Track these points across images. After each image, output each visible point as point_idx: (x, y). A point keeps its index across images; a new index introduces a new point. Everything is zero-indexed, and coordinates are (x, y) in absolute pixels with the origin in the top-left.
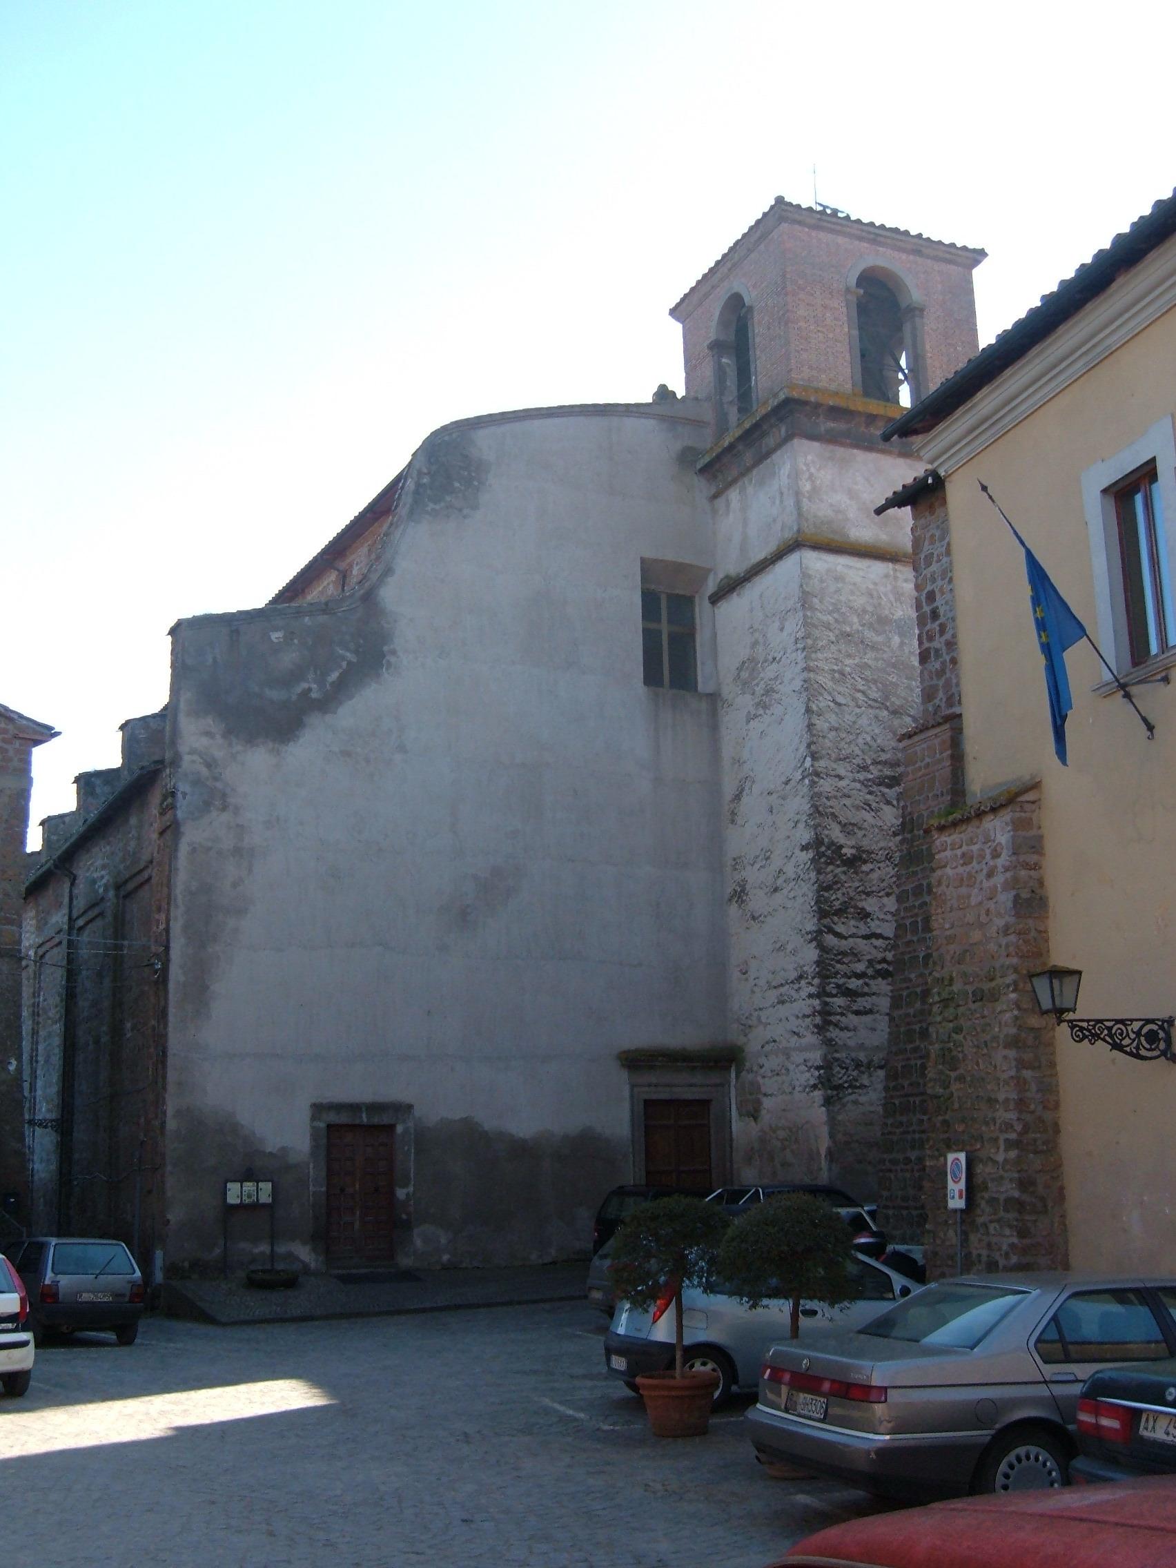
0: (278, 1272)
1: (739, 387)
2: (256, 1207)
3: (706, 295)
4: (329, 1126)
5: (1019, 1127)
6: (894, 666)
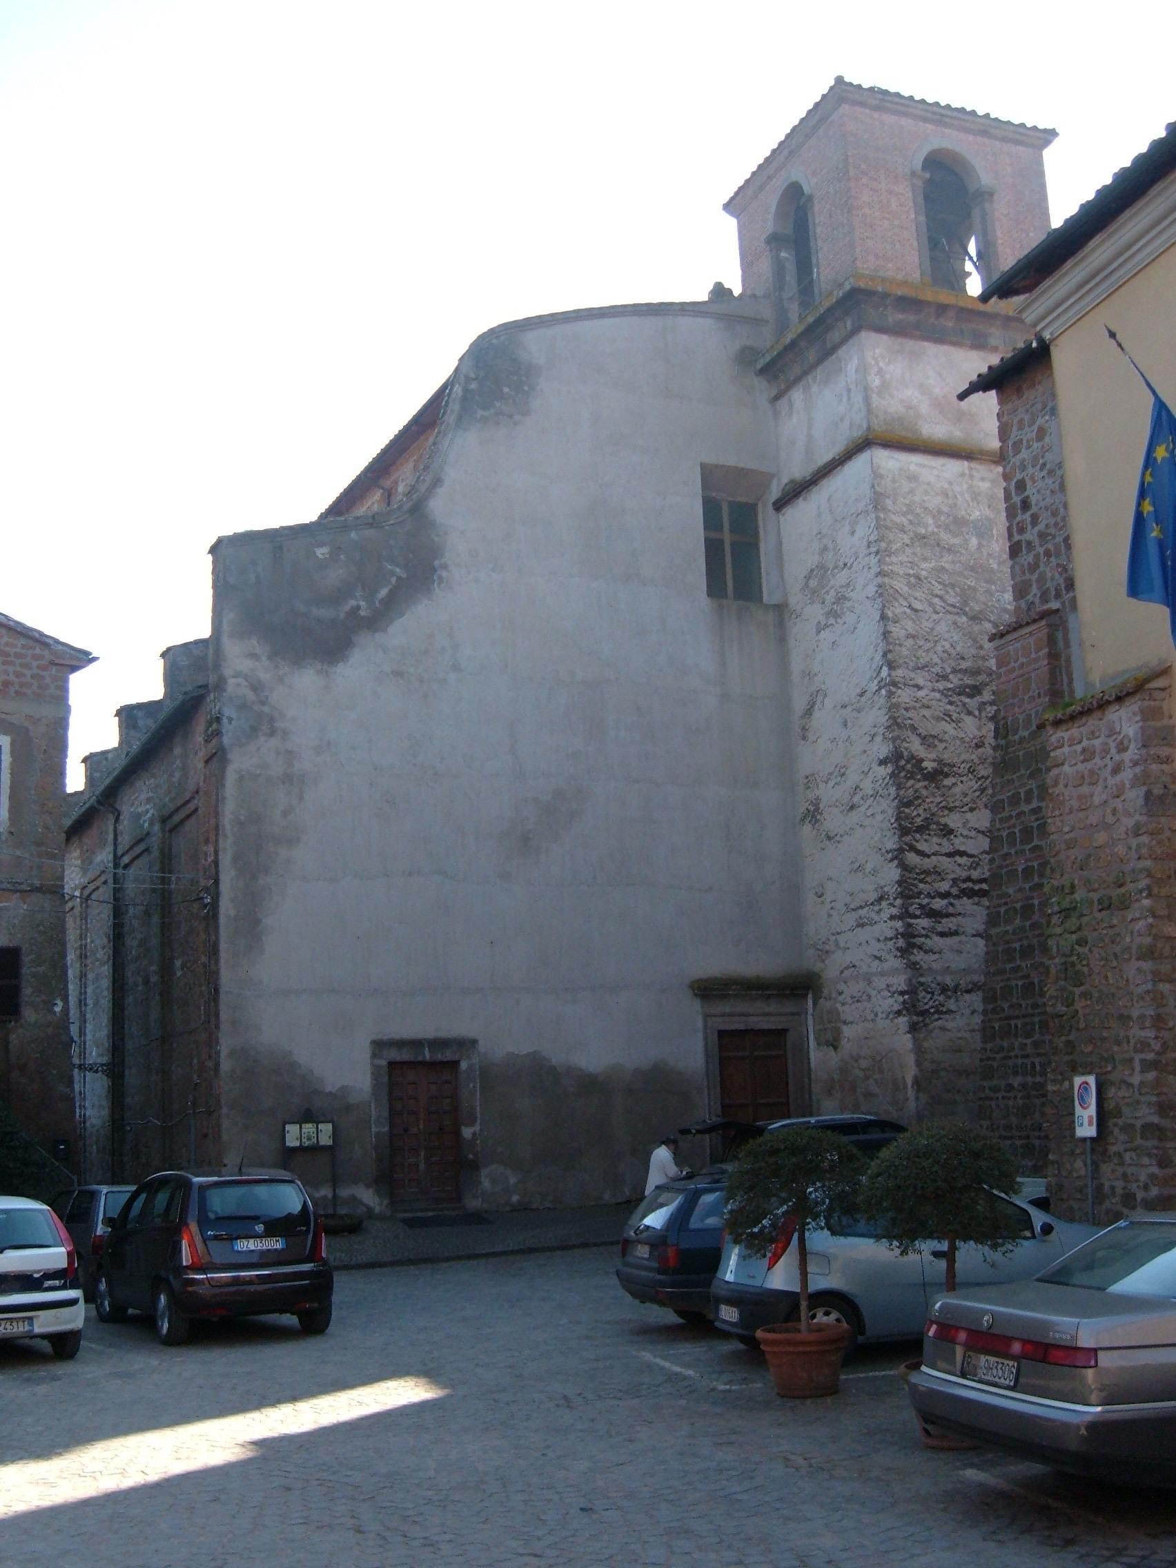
0: (341, 1217)
1: (799, 282)
2: (316, 1149)
3: (762, 188)
4: (390, 1063)
5: (1157, 1046)
6: (972, 569)
